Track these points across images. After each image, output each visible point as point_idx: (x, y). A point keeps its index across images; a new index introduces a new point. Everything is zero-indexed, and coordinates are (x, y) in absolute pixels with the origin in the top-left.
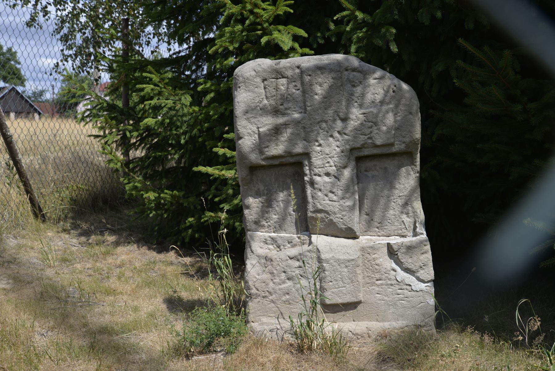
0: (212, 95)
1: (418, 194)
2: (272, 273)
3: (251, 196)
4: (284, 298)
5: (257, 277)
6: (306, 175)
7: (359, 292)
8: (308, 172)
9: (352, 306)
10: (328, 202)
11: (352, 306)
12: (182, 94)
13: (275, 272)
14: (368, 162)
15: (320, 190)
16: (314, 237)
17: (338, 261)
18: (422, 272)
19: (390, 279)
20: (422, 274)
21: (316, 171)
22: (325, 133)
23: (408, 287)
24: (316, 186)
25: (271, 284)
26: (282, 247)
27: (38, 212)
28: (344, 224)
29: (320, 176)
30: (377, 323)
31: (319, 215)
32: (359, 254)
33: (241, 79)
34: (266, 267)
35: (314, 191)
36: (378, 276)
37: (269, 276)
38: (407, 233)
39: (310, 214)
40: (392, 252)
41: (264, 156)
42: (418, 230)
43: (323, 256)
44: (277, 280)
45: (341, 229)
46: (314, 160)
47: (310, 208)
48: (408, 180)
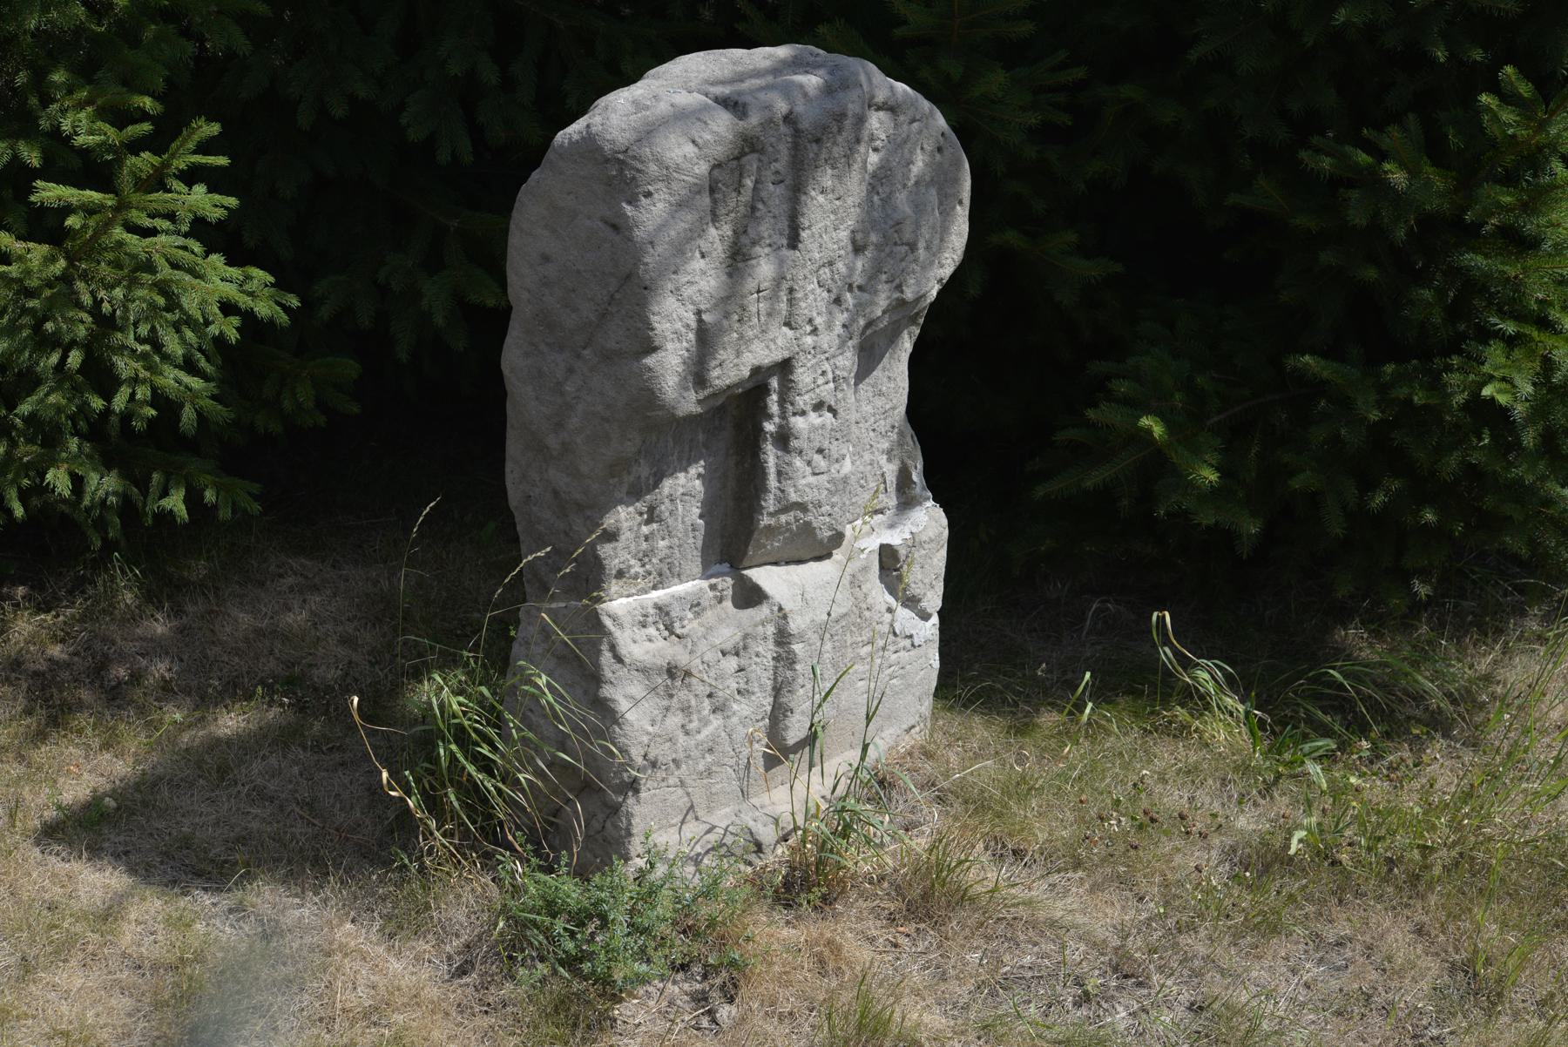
0: (146, 127)
3: (621, 502)
5: (650, 729)
6: (770, 417)
8: (774, 408)
24: (794, 443)
33: (653, 168)
34: (671, 696)
35: (787, 458)
41: (706, 392)
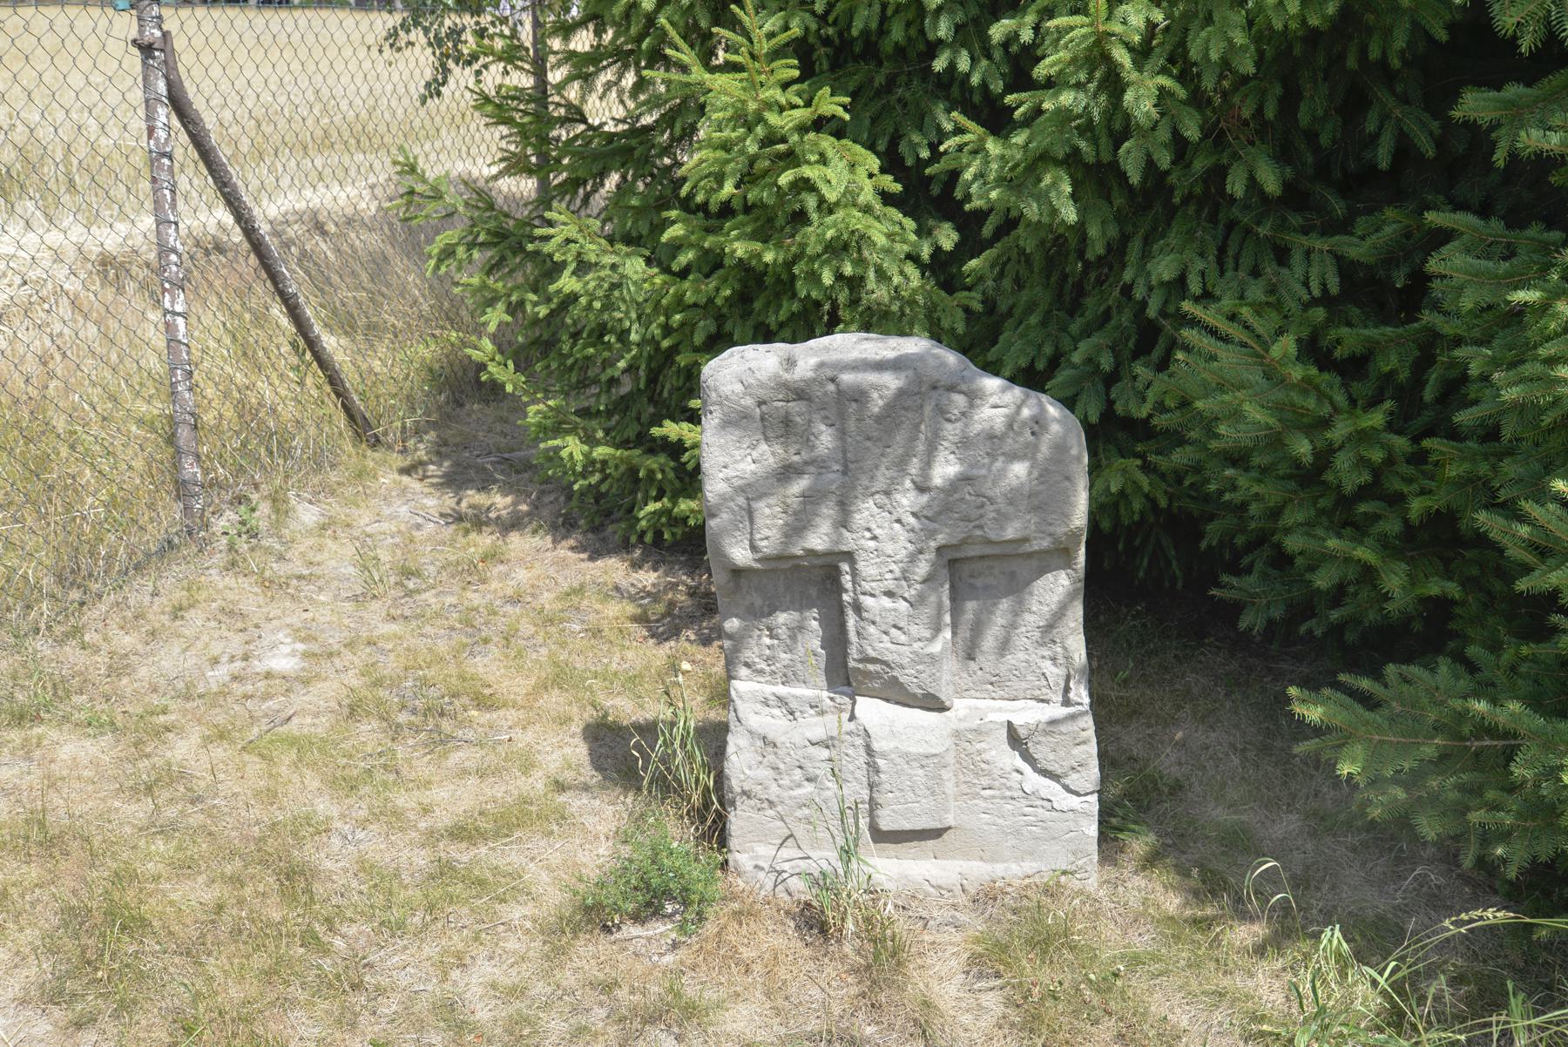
0: (691, 255)
1: (1077, 612)
2: (776, 769)
4: (799, 813)
6: (846, 591)
7: (947, 811)
8: (849, 586)
9: (937, 833)
10: (889, 645)
11: (937, 833)
12: (628, 255)
13: (782, 766)
14: (970, 571)
15: (874, 623)
16: (861, 701)
17: (908, 758)
18: (1075, 776)
19: (1010, 788)
20: (1073, 780)
21: (866, 586)
22: (886, 514)
23: (1046, 804)
24: (865, 615)
25: (774, 788)
26: (797, 714)
27: (362, 427)
28: (920, 687)
29: (873, 595)
30: (981, 864)
31: (871, 667)
32: (949, 742)
33: (714, 395)
36: (985, 782)
37: (770, 773)
38: (1051, 695)
39: (852, 664)
40: (1015, 739)
42: (1072, 695)
43: (876, 746)
44: (785, 782)
45: (914, 695)
46: (861, 565)
47: (853, 652)
48: (1058, 588)
